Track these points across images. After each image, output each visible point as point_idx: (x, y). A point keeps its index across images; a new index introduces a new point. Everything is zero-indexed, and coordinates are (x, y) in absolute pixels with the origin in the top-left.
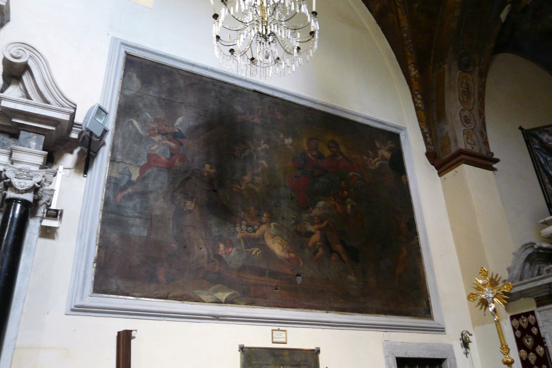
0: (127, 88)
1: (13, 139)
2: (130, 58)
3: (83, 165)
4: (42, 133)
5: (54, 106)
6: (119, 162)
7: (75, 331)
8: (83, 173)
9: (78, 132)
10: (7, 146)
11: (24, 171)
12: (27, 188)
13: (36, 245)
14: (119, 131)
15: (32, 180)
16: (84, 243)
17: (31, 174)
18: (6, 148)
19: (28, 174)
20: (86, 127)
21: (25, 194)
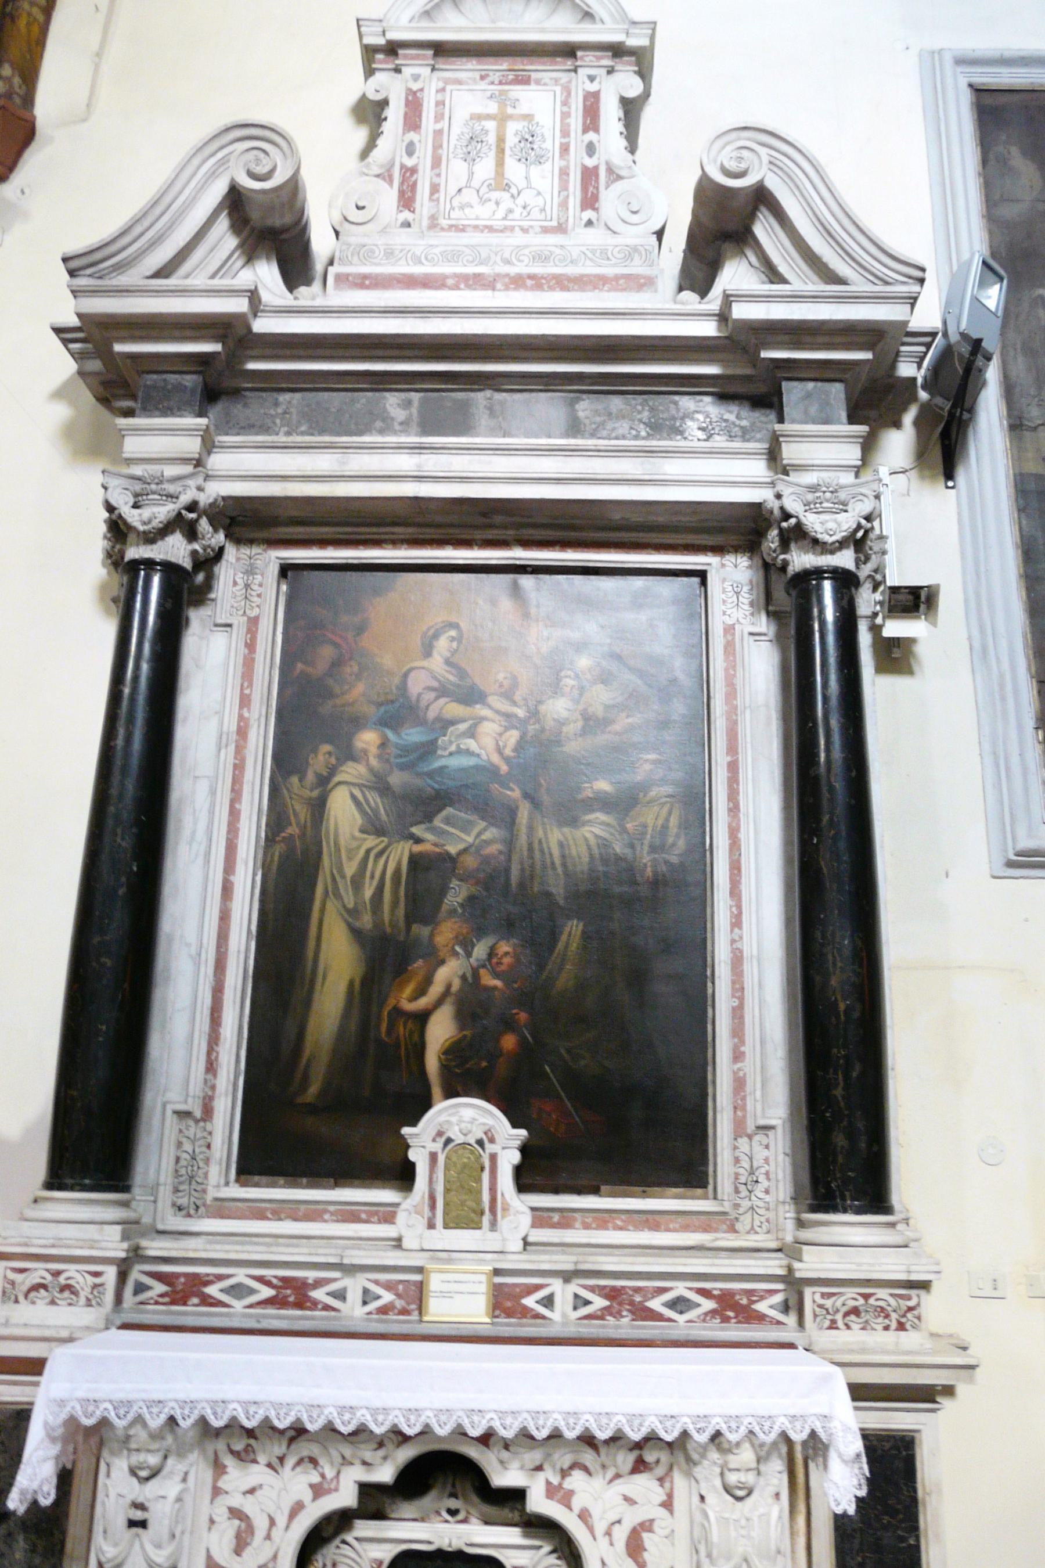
0: (1004, 200)
1: (763, 411)
2: (988, 100)
3: (936, 454)
4: (838, 376)
5: (860, 284)
6: (1035, 429)
7: (1026, 920)
8: (942, 479)
9: (916, 357)
10: (753, 434)
11: (824, 489)
12: (844, 534)
13: (874, 693)
14: (1011, 335)
15: (846, 511)
16: (1002, 676)
17: (842, 495)
18: (753, 438)
19: (836, 497)
20: (961, 330)
21: (839, 554)
